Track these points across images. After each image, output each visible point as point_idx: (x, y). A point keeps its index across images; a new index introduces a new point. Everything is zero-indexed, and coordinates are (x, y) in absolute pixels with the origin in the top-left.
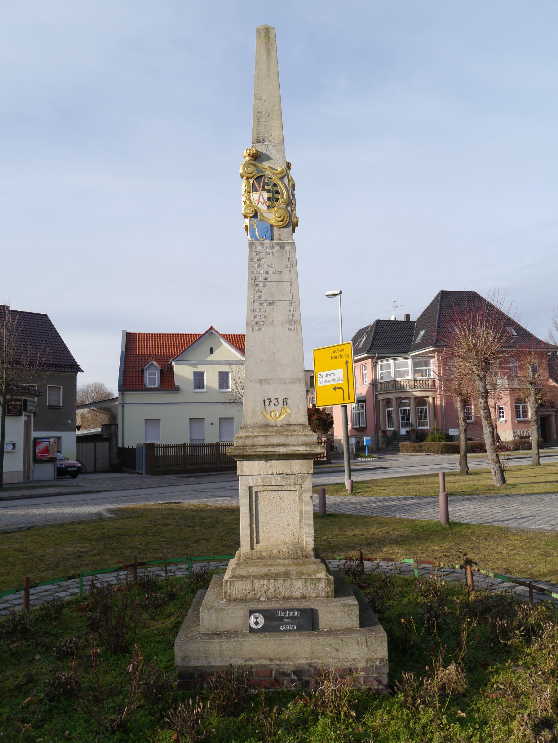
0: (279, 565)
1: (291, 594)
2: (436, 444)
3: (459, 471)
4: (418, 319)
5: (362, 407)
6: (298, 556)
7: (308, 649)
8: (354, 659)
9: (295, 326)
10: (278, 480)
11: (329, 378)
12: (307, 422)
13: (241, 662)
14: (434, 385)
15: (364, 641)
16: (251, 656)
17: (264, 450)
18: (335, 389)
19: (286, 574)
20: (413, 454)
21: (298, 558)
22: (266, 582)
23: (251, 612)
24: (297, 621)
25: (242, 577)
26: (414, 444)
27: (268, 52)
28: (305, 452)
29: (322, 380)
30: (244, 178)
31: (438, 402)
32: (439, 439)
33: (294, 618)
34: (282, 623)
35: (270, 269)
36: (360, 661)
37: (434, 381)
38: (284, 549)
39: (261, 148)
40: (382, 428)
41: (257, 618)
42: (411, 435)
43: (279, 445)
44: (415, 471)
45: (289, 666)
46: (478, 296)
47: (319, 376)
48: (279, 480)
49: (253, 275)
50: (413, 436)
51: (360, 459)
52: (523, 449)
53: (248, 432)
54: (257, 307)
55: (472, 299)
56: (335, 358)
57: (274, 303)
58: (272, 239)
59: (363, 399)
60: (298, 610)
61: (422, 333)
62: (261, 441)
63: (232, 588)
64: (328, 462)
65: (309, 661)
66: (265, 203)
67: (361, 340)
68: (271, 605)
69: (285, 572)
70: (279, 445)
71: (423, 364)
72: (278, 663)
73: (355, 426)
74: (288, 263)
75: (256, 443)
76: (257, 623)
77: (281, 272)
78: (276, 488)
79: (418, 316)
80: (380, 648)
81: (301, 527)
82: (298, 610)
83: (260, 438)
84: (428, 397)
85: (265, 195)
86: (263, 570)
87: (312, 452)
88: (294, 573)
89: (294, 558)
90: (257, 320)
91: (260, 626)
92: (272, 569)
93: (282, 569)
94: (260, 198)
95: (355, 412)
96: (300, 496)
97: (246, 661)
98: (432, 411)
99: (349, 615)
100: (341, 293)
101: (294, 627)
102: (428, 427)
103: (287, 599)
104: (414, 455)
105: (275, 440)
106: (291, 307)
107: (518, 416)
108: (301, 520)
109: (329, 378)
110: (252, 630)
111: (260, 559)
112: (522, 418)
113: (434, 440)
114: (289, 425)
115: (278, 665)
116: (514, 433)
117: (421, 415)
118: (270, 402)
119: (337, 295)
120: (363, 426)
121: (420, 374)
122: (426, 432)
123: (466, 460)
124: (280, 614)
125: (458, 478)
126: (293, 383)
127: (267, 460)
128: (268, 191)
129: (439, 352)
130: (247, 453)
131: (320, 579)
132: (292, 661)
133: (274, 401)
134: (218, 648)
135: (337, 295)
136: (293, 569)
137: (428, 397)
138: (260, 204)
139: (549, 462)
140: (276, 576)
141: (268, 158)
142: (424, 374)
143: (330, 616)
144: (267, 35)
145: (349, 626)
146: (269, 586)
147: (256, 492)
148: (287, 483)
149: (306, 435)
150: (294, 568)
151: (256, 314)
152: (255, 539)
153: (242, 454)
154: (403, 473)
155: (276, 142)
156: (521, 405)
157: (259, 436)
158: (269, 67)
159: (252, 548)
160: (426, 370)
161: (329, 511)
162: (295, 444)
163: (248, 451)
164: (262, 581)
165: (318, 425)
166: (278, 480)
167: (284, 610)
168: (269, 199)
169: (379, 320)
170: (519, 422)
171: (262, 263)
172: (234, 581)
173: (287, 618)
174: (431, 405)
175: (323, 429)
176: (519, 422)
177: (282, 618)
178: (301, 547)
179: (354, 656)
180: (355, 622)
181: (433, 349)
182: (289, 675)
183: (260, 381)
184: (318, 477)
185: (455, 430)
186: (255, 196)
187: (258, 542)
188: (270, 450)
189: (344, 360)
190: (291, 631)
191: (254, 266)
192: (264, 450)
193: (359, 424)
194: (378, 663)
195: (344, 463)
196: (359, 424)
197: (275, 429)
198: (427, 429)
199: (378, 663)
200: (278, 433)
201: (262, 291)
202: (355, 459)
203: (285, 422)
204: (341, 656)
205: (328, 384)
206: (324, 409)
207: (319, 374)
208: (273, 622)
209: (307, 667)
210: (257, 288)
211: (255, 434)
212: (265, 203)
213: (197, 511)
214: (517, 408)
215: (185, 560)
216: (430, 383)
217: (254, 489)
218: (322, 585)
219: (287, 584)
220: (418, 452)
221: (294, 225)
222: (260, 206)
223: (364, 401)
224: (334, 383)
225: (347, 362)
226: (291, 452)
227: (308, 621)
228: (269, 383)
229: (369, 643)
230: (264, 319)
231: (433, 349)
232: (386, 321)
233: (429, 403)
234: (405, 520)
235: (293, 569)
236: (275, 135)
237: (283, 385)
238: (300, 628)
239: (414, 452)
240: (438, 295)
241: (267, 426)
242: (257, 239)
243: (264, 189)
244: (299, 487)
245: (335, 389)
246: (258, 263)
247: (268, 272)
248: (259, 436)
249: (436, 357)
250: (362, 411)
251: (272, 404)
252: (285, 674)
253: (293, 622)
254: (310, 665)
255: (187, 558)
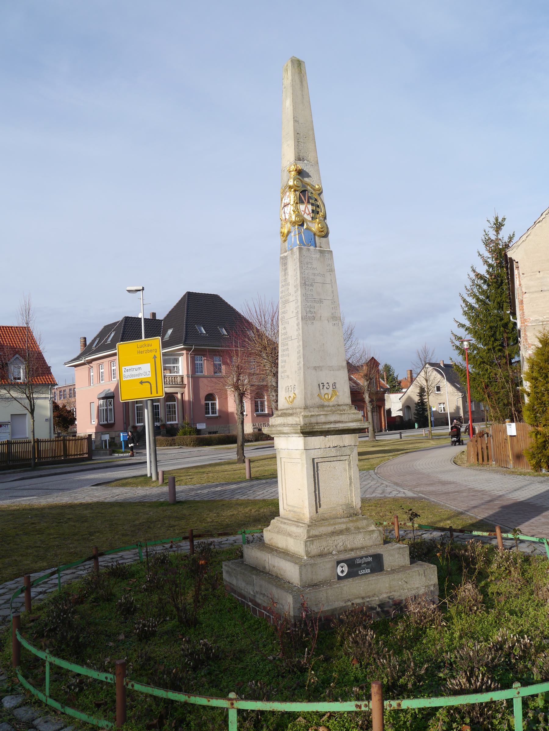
0: (340, 523)
1: (354, 546)
2: (188, 438)
3: (236, 461)
4: (165, 318)
5: (110, 403)
6: (352, 514)
7: (387, 585)
8: (417, 588)
9: (337, 322)
10: (333, 452)
11: (135, 372)
12: (351, 403)
13: (343, 604)
14: (182, 381)
15: (422, 572)
16: (349, 597)
17: (328, 426)
18: (141, 383)
19: (348, 530)
20: (166, 447)
21: (351, 516)
22: (336, 538)
23: (338, 563)
24: (370, 565)
25: (316, 536)
26: (167, 438)
27: (301, 82)
28: (357, 427)
29: (127, 374)
30: (292, 190)
31: (186, 398)
32: (190, 433)
33: (368, 563)
34: (360, 568)
35: (316, 272)
36: (421, 589)
37: (182, 377)
38: (340, 511)
39: (300, 166)
40: (131, 424)
41: (342, 567)
42: (162, 429)
43: (336, 422)
44: (188, 463)
45: (375, 601)
46: (221, 299)
47: (123, 370)
48: (334, 452)
49: (304, 276)
50: (163, 431)
51: (117, 455)
52: (261, 440)
53: (310, 412)
54: (308, 304)
55: (214, 301)
56: (142, 352)
57: (321, 301)
58: (316, 247)
59: (112, 395)
60: (370, 556)
61: (170, 332)
62: (322, 419)
63: (311, 546)
64: (90, 459)
65: (388, 595)
66: (309, 214)
67: (109, 336)
68: (352, 555)
69: (346, 528)
70: (336, 422)
71: (172, 362)
72: (368, 600)
73: (102, 423)
74: (329, 268)
75: (319, 421)
76: (342, 572)
77: (323, 275)
78: (332, 459)
79: (165, 315)
80: (433, 577)
81: (351, 490)
82: (370, 556)
83: (322, 417)
84: (177, 393)
85: (310, 207)
86: (330, 529)
87: (362, 427)
88: (352, 528)
89: (347, 517)
90: (309, 315)
91: (345, 574)
92: (337, 527)
93: (344, 526)
94: (306, 209)
95: (102, 408)
96: (349, 464)
97: (345, 603)
98: (180, 407)
99: (403, 555)
100: (143, 289)
101: (368, 571)
102: (176, 422)
103: (352, 550)
104: (168, 449)
105: (332, 418)
106: (333, 306)
107: (257, 410)
108: (350, 484)
109: (135, 372)
110: (339, 578)
111: (323, 520)
112: (260, 412)
113: (185, 434)
114: (338, 405)
115: (368, 601)
116: (253, 425)
117: (170, 411)
118: (323, 386)
119: (140, 290)
120: (111, 422)
121: (168, 371)
122: (175, 426)
123: (243, 450)
124: (358, 561)
125: (234, 466)
126: (339, 370)
127: (325, 436)
128: (312, 204)
129: (188, 350)
130: (315, 430)
131: (374, 531)
132: (378, 597)
133: (326, 385)
134: (325, 595)
135: (140, 290)
136: (351, 525)
137: (177, 393)
138: (305, 214)
139: (263, 454)
140: (341, 532)
141: (308, 176)
142: (172, 371)
143: (390, 558)
144: (298, 64)
145: (404, 564)
146: (339, 541)
147: (317, 463)
148: (339, 456)
149: (354, 413)
150: (352, 524)
151: (308, 310)
152: (318, 503)
153: (311, 430)
154: (178, 465)
155: (313, 162)
156: (210, 402)
157: (320, 415)
158: (303, 95)
159: (317, 512)
160: (174, 367)
161: (180, 497)
162: (347, 420)
163: (317, 428)
164: (333, 538)
165: (59, 422)
166: (333, 452)
167: (361, 558)
168: (313, 211)
169: (128, 317)
170: (258, 416)
171: (309, 266)
172: (312, 540)
173: (364, 564)
174: (180, 401)
175: (63, 427)
176: (258, 416)
177: (360, 564)
178: (351, 507)
179: (417, 586)
180: (406, 560)
181: (183, 347)
182: (375, 609)
183: (315, 368)
184: (101, 472)
185: (202, 424)
186: (302, 207)
187: (320, 507)
188: (332, 426)
189: (153, 354)
190: (367, 574)
191: (304, 268)
192: (328, 426)
193: (107, 420)
194: (432, 588)
195: (145, 455)
196: (107, 420)
197: (329, 409)
198: (177, 424)
199: (432, 588)
200: (333, 412)
201: (311, 290)
202: (111, 455)
203: (336, 403)
204: (409, 587)
205: (134, 378)
206: (64, 406)
207: (123, 368)
208: (354, 567)
209: (388, 600)
210: (307, 287)
211: (317, 414)
212: (309, 214)
213: (52, 507)
214: (256, 403)
215: (136, 547)
216: (179, 380)
217: (316, 461)
218: (375, 535)
219: (351, 537)
220: (171, 446)
221: (326, 236)
222: (306, 216)
223: (113, 397)
224: (140, 377)
225: (155, 357)
226: (347, 428)
227: (376, 564)
228: (321, 370)
229: (426, 573)
230: (314, 315)
231: (183, 347)
232: (135, 318)
233: (178, 398)
234: (259, 500)
235: (351, 525)
236: (311, 157)
237: (332, 372)
238: (373, 571)
239: (167, 446)
240: (184, 296)
241: (323, 406)
242: (304, 245)
243: (308, 202)
244: (348, 457)
245: (141, 383)
246: (306, 265)
247: (314, 274)
248: (320, 415)
249: (185, 355)
250: (110, 407)
251: (325, 387)
252: (373, 609)
253: (368, 566)
254: (389, 597)
255: (137, 545)
